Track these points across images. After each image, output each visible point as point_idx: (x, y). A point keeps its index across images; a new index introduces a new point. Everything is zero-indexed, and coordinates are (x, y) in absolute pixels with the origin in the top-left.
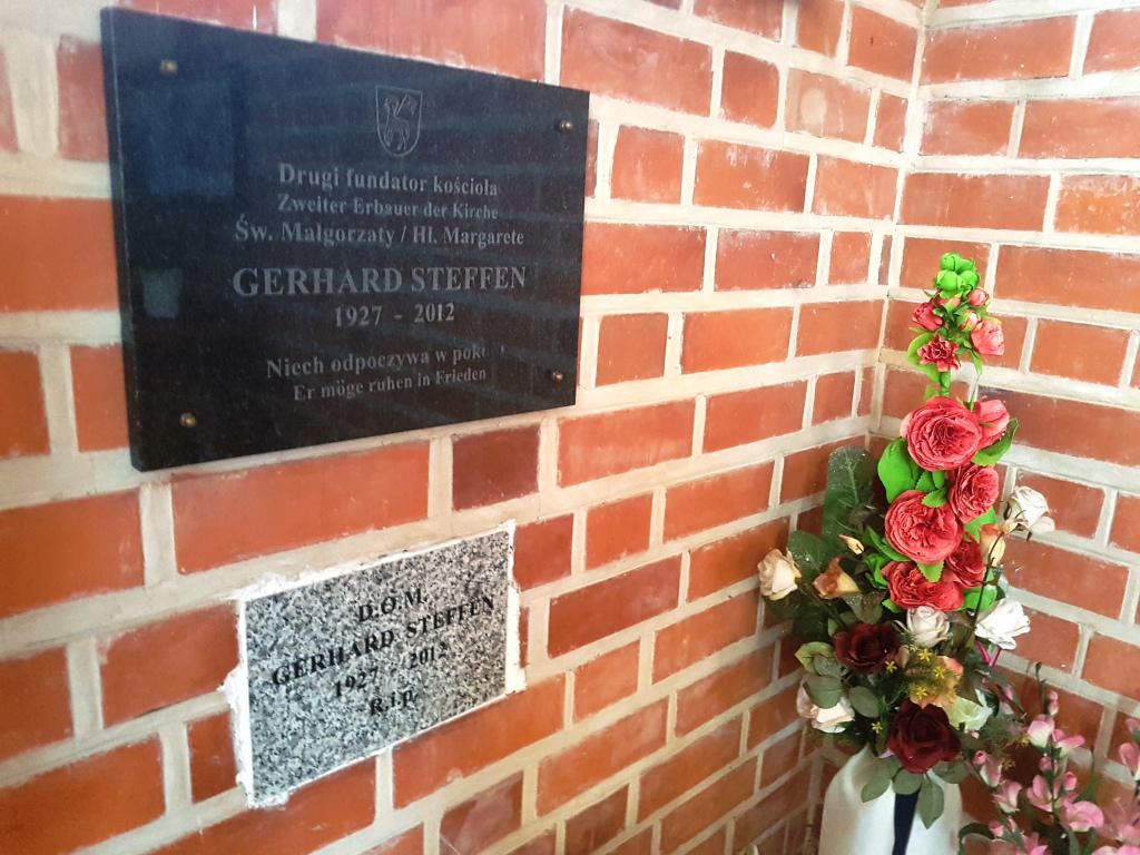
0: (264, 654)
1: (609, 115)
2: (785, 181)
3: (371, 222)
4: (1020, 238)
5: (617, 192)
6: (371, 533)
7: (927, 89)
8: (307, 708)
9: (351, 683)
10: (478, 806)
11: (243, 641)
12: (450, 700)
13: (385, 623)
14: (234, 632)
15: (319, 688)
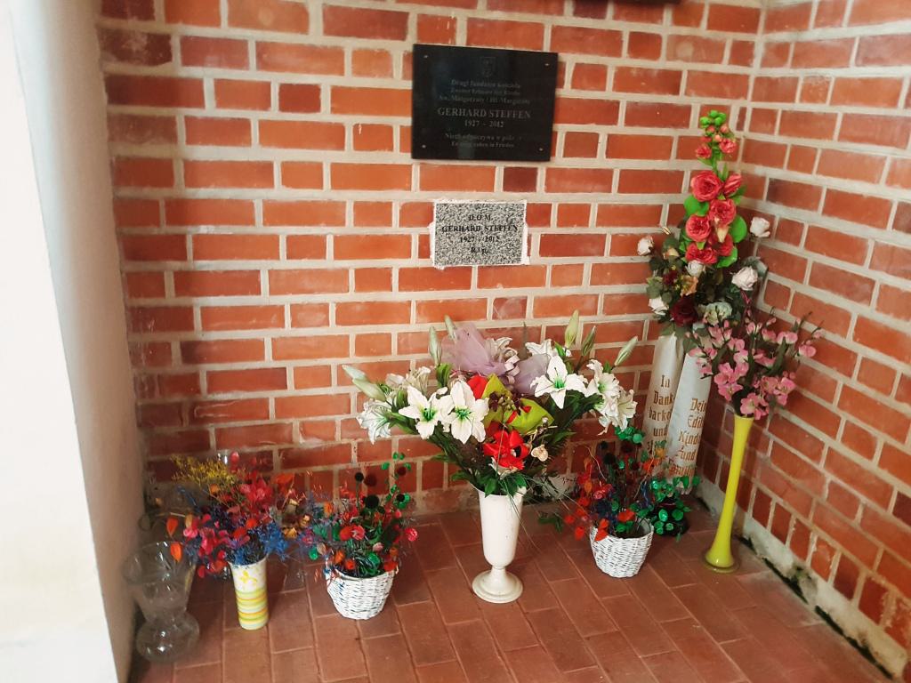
0: (440, 220)
1: (570, 60)
2: (669, 82)
3: (477, 96)
4: (787, 106)
5: (574, 86)
6: (475, 192)
7: (765, 36)
8: (452, 242)
9: (465, 239)
10: (507, 302)
11: (435, 216)
12: (500, 258)
13: (478, 223)
14: (432, 212)
15: (456, 237)
